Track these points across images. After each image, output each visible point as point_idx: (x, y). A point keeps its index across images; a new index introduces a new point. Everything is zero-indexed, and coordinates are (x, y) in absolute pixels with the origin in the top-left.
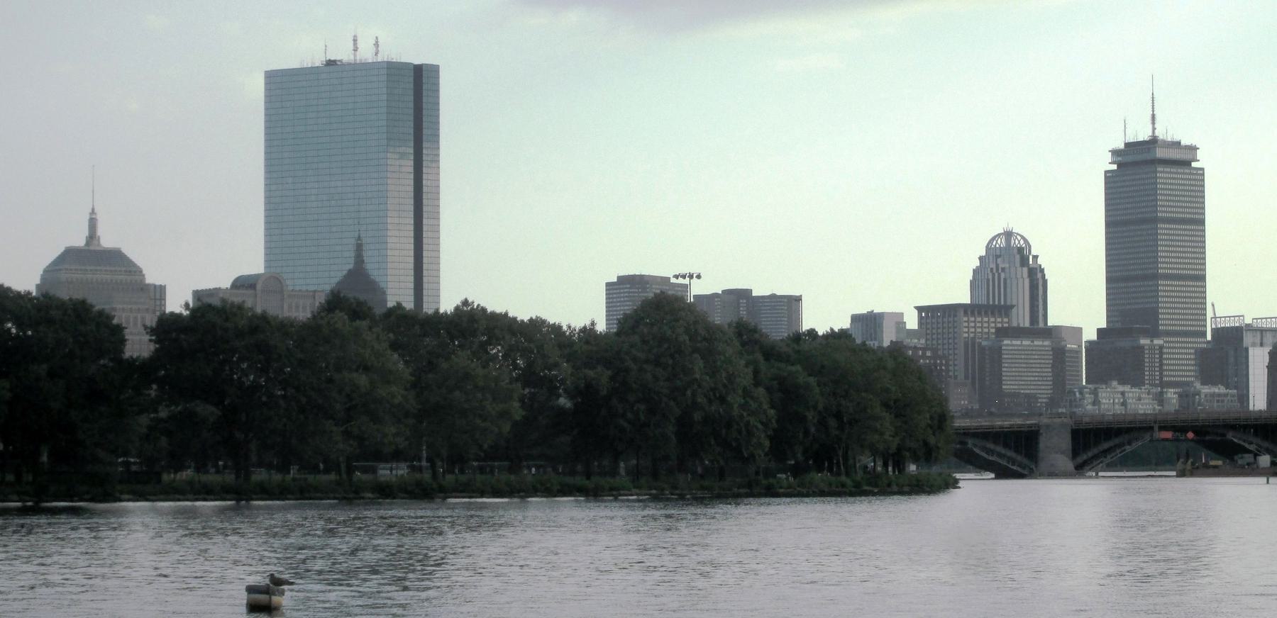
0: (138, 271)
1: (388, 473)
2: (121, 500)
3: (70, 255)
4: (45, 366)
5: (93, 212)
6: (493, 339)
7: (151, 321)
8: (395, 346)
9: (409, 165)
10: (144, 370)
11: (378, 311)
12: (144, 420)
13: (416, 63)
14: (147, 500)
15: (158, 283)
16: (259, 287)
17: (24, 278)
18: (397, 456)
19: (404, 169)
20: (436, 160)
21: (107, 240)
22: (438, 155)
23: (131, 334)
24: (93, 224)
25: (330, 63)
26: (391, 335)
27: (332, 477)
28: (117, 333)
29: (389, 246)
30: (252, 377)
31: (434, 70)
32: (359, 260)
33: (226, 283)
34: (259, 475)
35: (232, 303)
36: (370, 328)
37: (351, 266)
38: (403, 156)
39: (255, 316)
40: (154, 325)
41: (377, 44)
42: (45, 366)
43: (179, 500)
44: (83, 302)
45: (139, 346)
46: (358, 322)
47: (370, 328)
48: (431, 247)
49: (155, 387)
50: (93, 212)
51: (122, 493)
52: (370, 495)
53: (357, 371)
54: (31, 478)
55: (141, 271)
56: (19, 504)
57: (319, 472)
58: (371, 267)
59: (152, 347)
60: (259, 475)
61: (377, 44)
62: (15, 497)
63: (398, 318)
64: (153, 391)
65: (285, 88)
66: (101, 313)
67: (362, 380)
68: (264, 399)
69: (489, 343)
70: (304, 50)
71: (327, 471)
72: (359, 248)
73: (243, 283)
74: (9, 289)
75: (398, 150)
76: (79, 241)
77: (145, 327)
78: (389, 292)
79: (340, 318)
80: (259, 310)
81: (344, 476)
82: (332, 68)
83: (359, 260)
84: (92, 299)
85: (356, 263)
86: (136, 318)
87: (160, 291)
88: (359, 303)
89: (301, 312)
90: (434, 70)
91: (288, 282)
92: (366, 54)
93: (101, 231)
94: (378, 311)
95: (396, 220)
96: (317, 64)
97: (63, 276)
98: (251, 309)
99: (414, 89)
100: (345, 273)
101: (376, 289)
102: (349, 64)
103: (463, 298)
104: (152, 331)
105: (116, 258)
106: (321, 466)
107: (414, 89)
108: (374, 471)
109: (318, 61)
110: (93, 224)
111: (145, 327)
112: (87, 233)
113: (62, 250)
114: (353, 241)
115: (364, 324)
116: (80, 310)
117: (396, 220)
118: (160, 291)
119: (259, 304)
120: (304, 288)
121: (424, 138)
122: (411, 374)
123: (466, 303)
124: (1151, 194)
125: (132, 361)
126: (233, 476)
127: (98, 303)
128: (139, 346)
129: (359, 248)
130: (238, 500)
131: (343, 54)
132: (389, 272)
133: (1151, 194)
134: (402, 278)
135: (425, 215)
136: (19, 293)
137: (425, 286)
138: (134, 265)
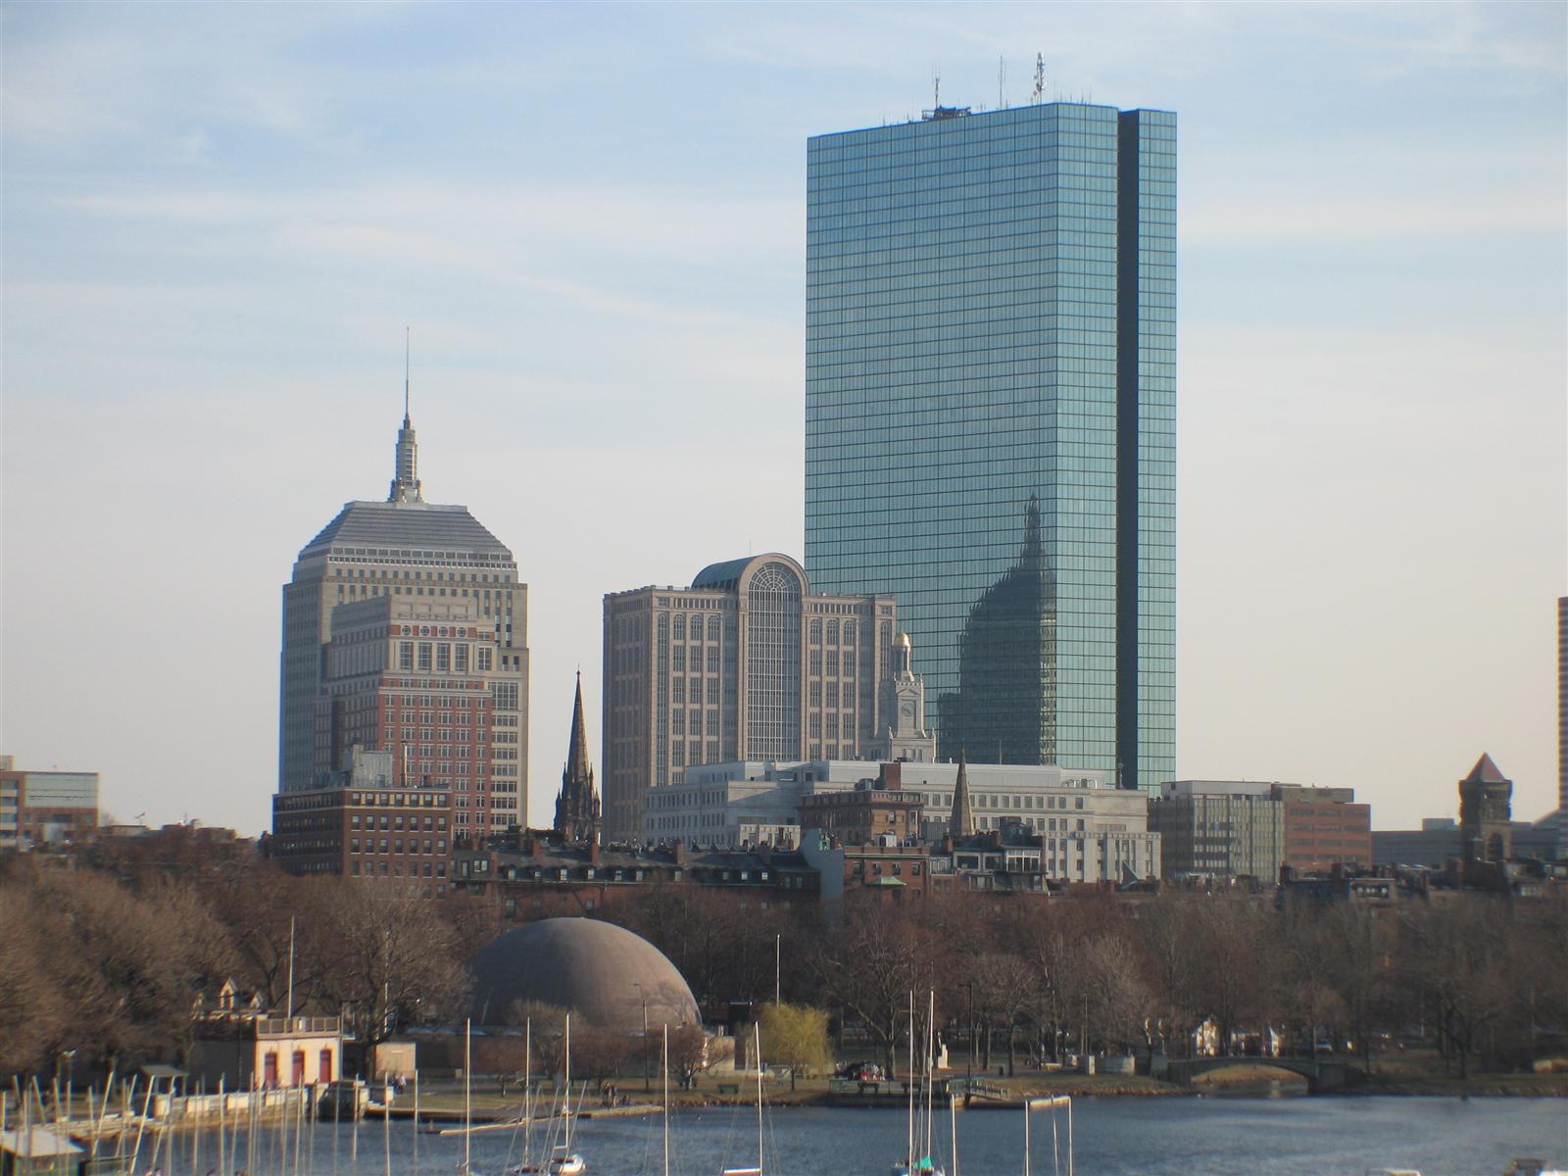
3: (352, 520)
21: (439, 487)
25: (943, 114)
82: (947, 124)
85: (1025, 555)
90: (1168, 121)
93: (422, 470)
105: (456, 527)
137: (1143, 594)
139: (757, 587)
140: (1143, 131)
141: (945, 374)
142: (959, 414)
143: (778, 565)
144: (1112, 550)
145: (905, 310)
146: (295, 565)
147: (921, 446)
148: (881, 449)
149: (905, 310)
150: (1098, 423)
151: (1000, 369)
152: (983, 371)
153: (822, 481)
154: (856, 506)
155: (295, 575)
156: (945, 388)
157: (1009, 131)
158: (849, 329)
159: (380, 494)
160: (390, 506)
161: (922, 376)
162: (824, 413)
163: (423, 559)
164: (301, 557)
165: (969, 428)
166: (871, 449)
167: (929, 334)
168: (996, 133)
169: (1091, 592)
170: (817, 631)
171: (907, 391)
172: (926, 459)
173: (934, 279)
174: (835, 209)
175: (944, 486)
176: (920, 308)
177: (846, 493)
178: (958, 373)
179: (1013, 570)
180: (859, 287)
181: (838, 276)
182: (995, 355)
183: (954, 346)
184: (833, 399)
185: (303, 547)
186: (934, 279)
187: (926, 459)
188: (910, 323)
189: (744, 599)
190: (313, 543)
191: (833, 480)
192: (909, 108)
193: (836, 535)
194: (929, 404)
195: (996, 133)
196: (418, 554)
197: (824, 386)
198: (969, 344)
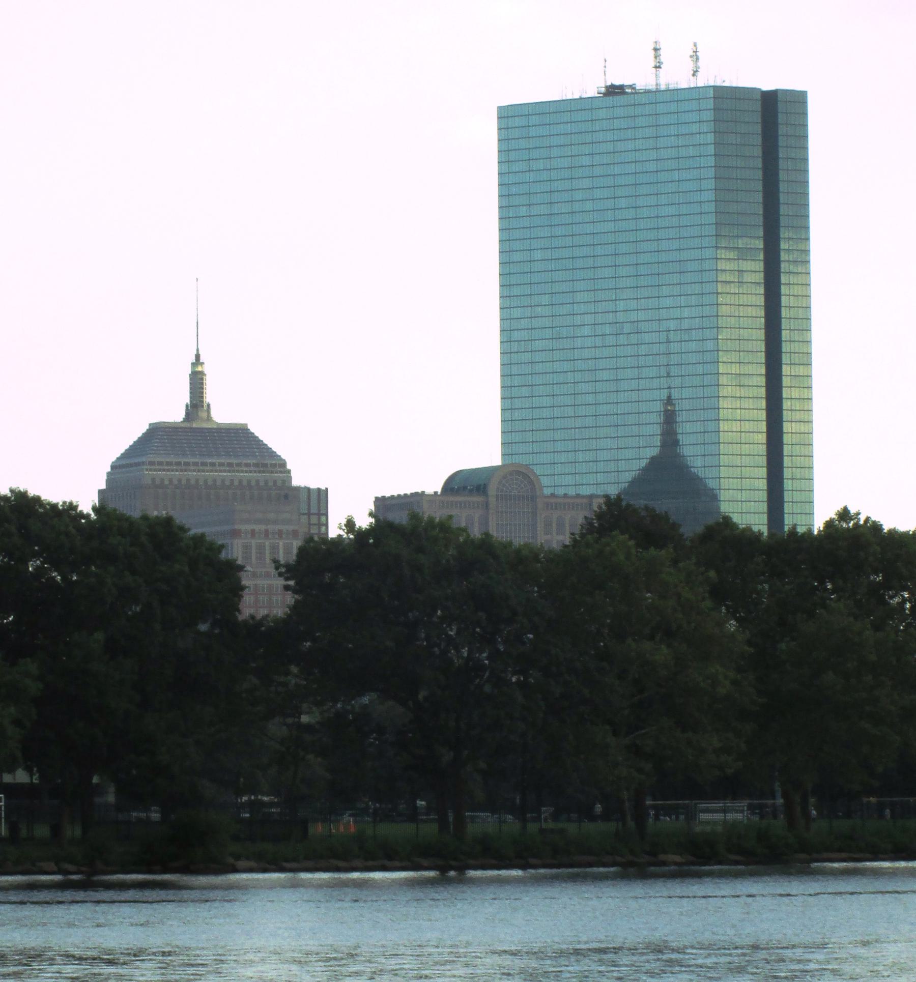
0: (281, 465)
1: (715, 816)
2: (235, 870)
3: (157, 436)
4: (99, 636)
5: (198, 360)
6: (894, 581)
7: (288, 549)
8: (718, 593)
9: (755, 269)
10: (272, 639)
11: (690, 529)
12: (277, 728)
13: (767, 87)
14: (282, 870)
15: (313, 486)
16: (492, 491)
17: (74, 481)
18: (729, 788)
19: (748, 278)
20: (804, 260)
21: (223, 411)
22: (807, 252)
23: (254, 575)
24: (197, 382)
25: (613, 91)
26: (712, 574)
27: (611, 827)
28: (227, 576)
29: (723, 414)
30: (465, 652)
31: (798, 100)
32: (670, 439)
33: (433, 485)
34: (483, 823)
35: (431, 520)
36: (675, 562)
37: (655, 452)
38: (743, 254)
39: (470, 542)
40: (293, 558)
41: (695, 57)
42: (99, 636)
43: (338, 869)
44: (169, 521)
45: (265, 596)
46: (653, 551)
47: (675, 562)
48: (798, 416)
49: (294, 669)
50: (198, 360)
51: (238, 857)
52: (678, 859)
53: (652, 638)
54: (78, 832)
55: (283, 464)
56: (58, 878)
57: (593, 818)
58: (691, 451)
59: (290, 599)
60: (483, 823)
61: (695, 57)
62: (52, 866)
63: (725, 539)
64: (294, 676)
65: (534, 140)
66: (199, 540)
67: (662, 654)
68: (487, 688)
69: (886, 585)
70: (569, 74)
71: (606, 817)
72: (669, 418)
73: (462, 485)
74: (37, 500)
75: (741, 243)
76: (176, 415)
77: (276, 562)
78: (724, 495)
79: (621, 543)
80: (476, 533)
81: (631, 824)
82: (618, 100)
83: (670, 439)
84: (180, 518)
85: (664, 445)
86: (261, 548)
87: (317, 500)
88: (657, 518)
89: (554, 536)
90: (798, 100)
91: (545, 481)
92: (677, 76)
93: (210, 396)
94: (690, 529)
95: (735, 369)
96: (592, 92)
97: (148, 474)
98: (464, 530)
99: (763, 137)
100: (644, 463)
101: (699, 492)
102: (648, 92)
103: (839, 507)
104: (289, 571)
105: (239, 440)
106: (598, 808)
107: (763, 137)
108: (691, 815)
109: (592, 88)
110: (197, 382)
111: (276, 562)
112: (187, 400)
113: (144, 428)
114: (658, 406)
115: (664, 554)
116: (163, 536)
117: (735, 369)
118: (317, 500)
119: (471, 521)
120: (572, 492)
121: (783, 221)
122: (749, 643)
123: (844, 514)
124: (671, 202)
125: (254, 627)
126: (435, 827)
127: (196, 522)
128: (265, 596)
129: (669, 418)
130: (443, 869)
131: (640, 77)
132: (724, 460)
133: (671, 202)
134: (746, 472)
135: (785, 358)
136: (54, 506)
137: (788, 484)
138: (272, 454)
139: (502, 491)
140: (781, 107)
141: (621, 305)
142: (634, 338)
143: (519, 473)
144: (763, 484)
145: (586, 251)
146: (108, 474)
147: (602, 364)
148: (566, 366)
149: (586, 251)
150: (750, 346)
151: (668, 302)
152: (652, 303)
153: (516, 392)
154: (546, 413)
155: (108, 481)
156: (621, 317)
157: (673, 107)
158: (538, 266)
159: (176, 415)
160: (187, 425)
161: (601, 307)
162: (516, 335)
163: (192, 468)
164: (113, 467)
165: (643, 350)
166: (557, 366)
167: (607, 272)
168: (661, 108)
169: (747, 483)
170: (548, 524)
171: (589, 319)
172: (605, 375)
173: (610, 226)
174: (522, 166)
175: (622, 397)
176: (599, 250)
177: (536, 402)
178: (633, 304)
179: (653, 458)
180: (546, 232)
181: (526, 222)
182: (665, 290)
183: (630, 282)
184: (524, 323)
185: (114, 459)
186: (610, 226)
187: (605, 375)
188: (590, 262)
189: (492, 500)
190: (124, 456)
191: (525, 391)
192: (590, 86)
193: (529, 437)
194: (607, 330)
195: (661, 108)
196: (213, 464)
197: (517, 313)
198: (642, 281)
